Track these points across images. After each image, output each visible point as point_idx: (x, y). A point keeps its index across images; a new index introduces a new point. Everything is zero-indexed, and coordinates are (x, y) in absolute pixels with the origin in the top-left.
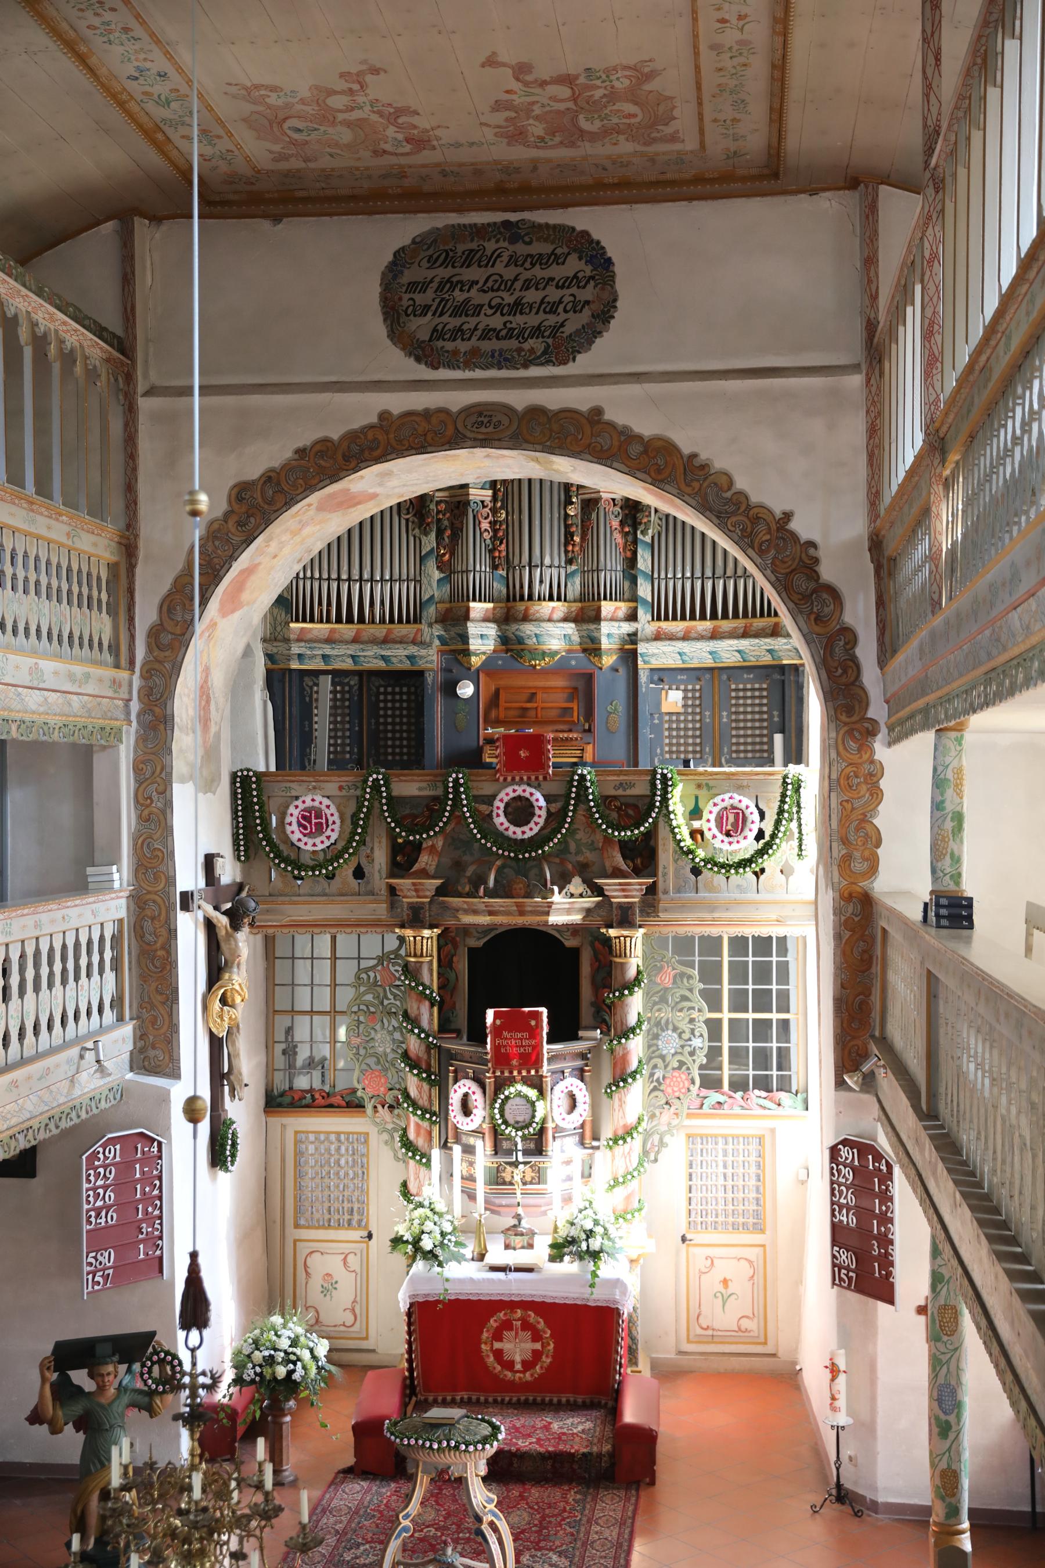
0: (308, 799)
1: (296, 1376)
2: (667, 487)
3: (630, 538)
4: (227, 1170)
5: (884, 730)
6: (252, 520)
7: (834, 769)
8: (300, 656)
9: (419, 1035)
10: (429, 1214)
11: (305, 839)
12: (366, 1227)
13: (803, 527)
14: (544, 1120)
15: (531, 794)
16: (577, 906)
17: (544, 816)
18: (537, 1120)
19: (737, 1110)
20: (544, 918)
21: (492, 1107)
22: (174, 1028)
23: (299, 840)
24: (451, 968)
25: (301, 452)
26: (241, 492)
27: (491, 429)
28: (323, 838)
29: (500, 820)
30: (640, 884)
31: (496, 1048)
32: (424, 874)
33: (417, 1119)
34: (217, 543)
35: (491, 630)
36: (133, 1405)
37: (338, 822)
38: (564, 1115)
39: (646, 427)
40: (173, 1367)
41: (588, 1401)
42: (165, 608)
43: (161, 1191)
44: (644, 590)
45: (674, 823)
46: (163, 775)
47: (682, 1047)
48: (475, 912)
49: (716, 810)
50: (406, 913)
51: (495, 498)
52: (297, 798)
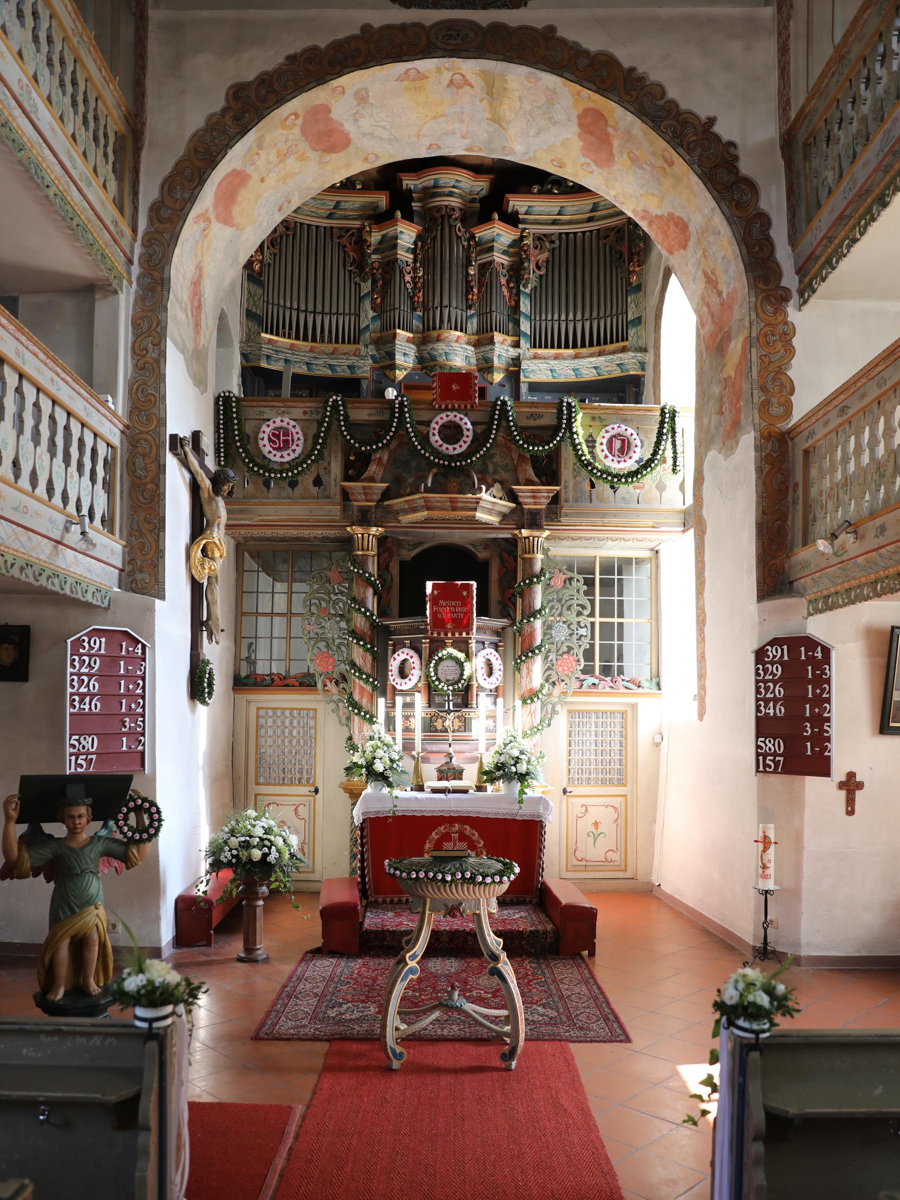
0: (278, 420)
1: (272, 858)
2: (610, 95)
3: (514, 291)
4: (204, 702)
5: (795, 295)
6: (247, 115)
7: (754, 328)
8: (268, 357)
9: (365, 613)
10: (379, 744)
11: (275, 452)
12: (313, 784)
13: (724, 130)
14: (470, 678)
15: (461, 419)
16: (497, 508)
17: (471, 438)
18: (465, 677)
19: (608, 690)
20: (471, 513)
21: (427, 666)
22: (160, 553)
23: (270, 452)
24: (388, 571)
25: (291, 58)
26: (238, 92)
27: (459, 41)
28: (290, 451)
29: (435, 439)
30: (548, 491)
31: (434, 614)
32: (372, 479)
33: (362, 683)
34: (215, 134)
35: (412, 350)
36: (108, 854)
37: (302, 438)
38: (485, 677)
39: (592, 43)
40: (151, 815)
41: (515, 899)
42: (166, 187)
43: (144, 691)
44: (525, 326)
45: (577, 441)
46: (159, 329)
47: (571, 635)
48: (414, 510)
49: (607, 436)
50: (356, 515)
51: (415, 260)
52: (269, 420)
